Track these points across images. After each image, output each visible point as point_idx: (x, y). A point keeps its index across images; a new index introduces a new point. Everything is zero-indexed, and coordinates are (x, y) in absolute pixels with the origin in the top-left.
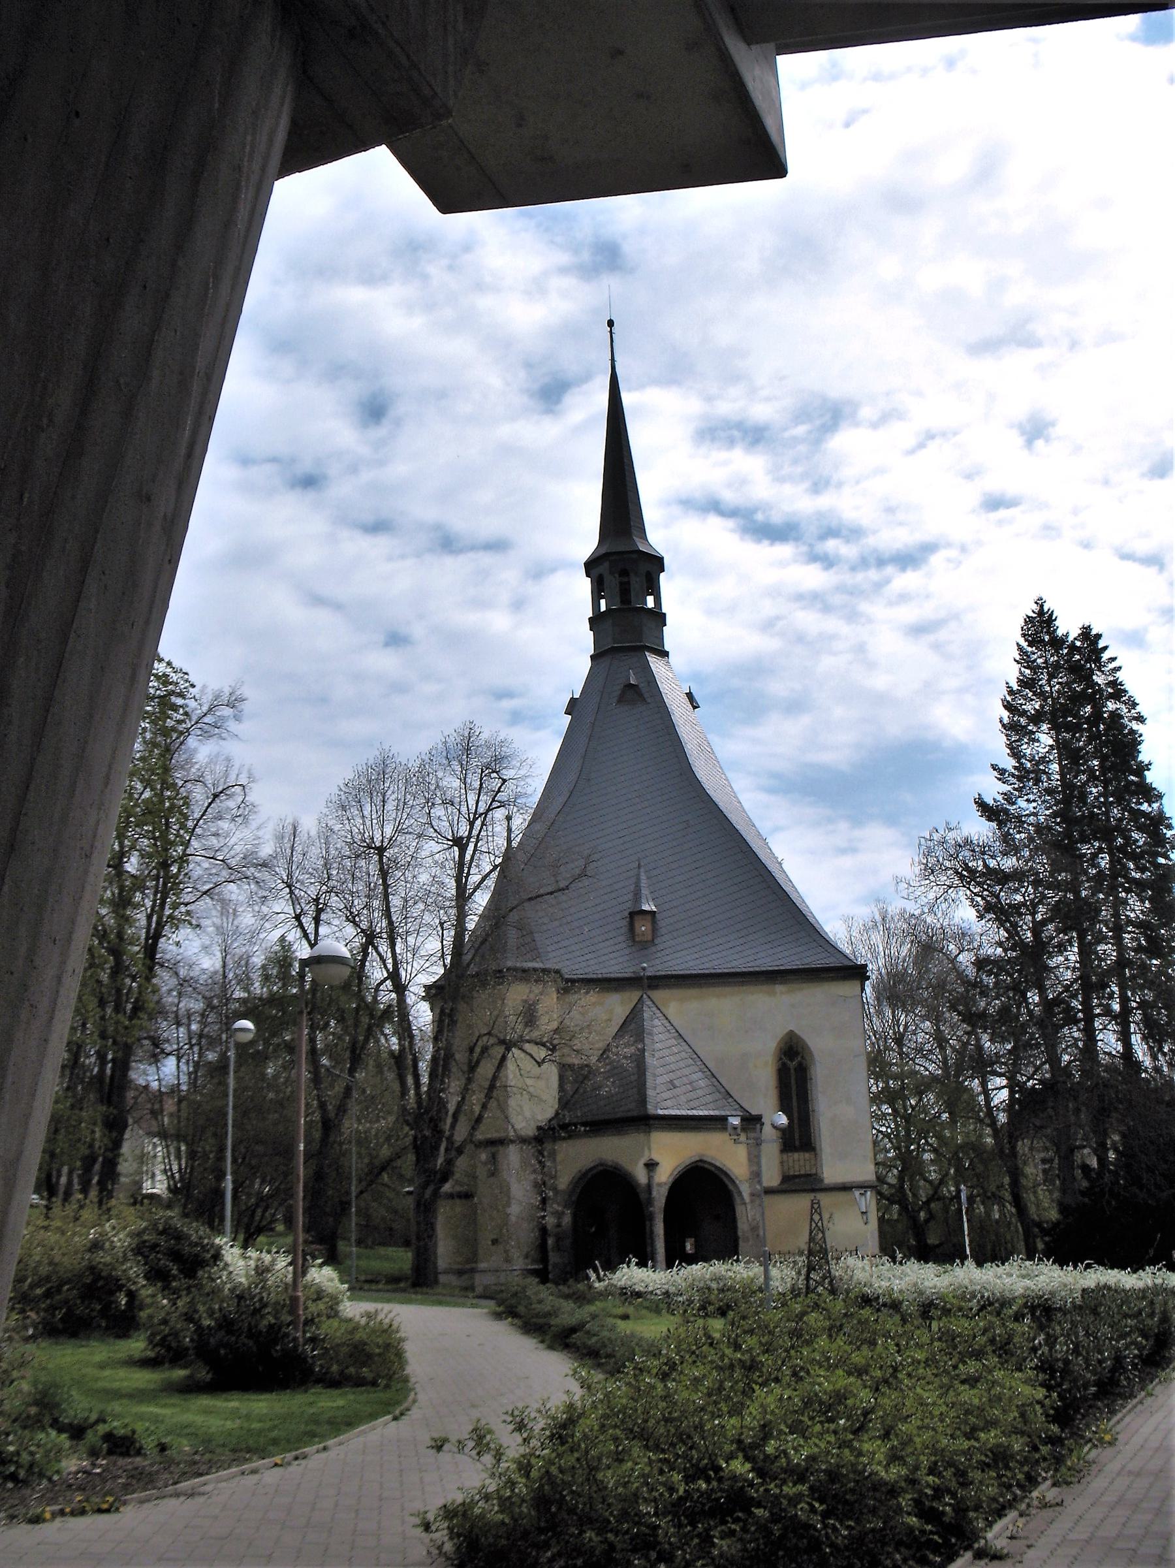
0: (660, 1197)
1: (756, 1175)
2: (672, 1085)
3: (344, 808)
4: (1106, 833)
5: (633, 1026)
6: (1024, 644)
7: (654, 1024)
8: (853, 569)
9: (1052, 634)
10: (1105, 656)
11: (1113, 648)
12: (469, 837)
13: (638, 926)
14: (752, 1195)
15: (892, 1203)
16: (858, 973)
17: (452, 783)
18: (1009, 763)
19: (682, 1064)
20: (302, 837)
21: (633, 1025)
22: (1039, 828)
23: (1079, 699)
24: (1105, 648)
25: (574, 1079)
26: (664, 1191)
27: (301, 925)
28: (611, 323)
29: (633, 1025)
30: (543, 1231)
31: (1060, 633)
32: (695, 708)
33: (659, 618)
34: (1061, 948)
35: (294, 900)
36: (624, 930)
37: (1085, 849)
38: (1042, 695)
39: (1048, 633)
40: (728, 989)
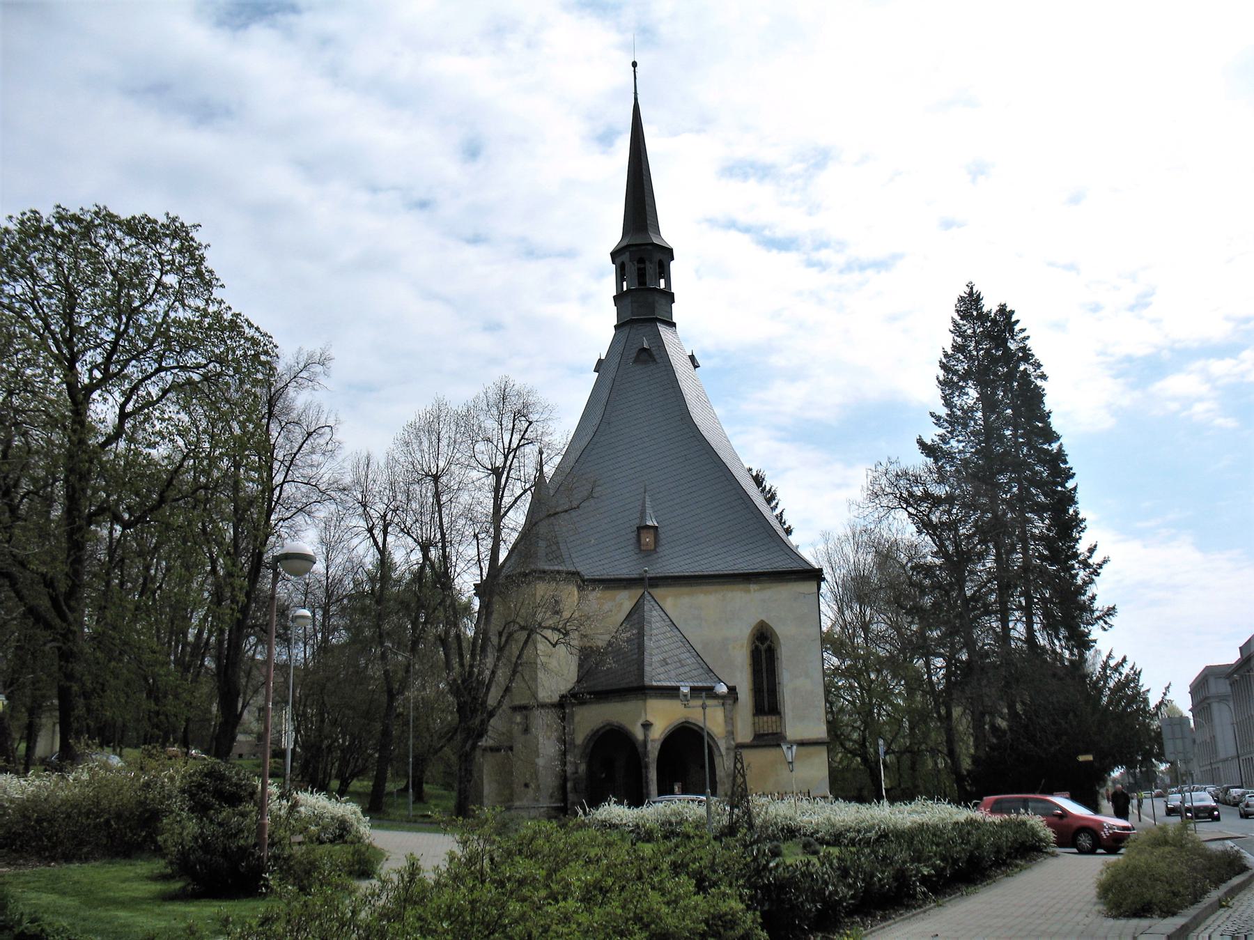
0: (653, 751)
1: (731, 734)
2: (665, 662)
3: (407, 444)
4: (1018, 466)
5: (635, 616)
6: (957, 318)
7: (653, 616)
8: (841, 272)
9: (979, 309)
10: (1017, 328)
11: (1024, 318)
12: (504, 467)
13: (645, 537)
14: (728, 749)
15: (855, 755)
16: (816, 575)
17: (490, 424)
18: (943, 412)
19: (673, 646)
20: (373, 467)
21: (636, 617)
22: (966, 462)
23: (995, 361)
24: (1017, 321)
25: (588, 658)
26: (657, 746)
27: (372, 535)
28: (634, 64)
29: (636, 617)
30: (564, 779)
31: (985, 310)
32: (696, 367)
33: (670, 297)
34: (981, 557)
35: (366, 516)
36: (634, 540)
37: (1003, 479)
38: (970, 358)
39: (977, 309)
40: (714, 588)
